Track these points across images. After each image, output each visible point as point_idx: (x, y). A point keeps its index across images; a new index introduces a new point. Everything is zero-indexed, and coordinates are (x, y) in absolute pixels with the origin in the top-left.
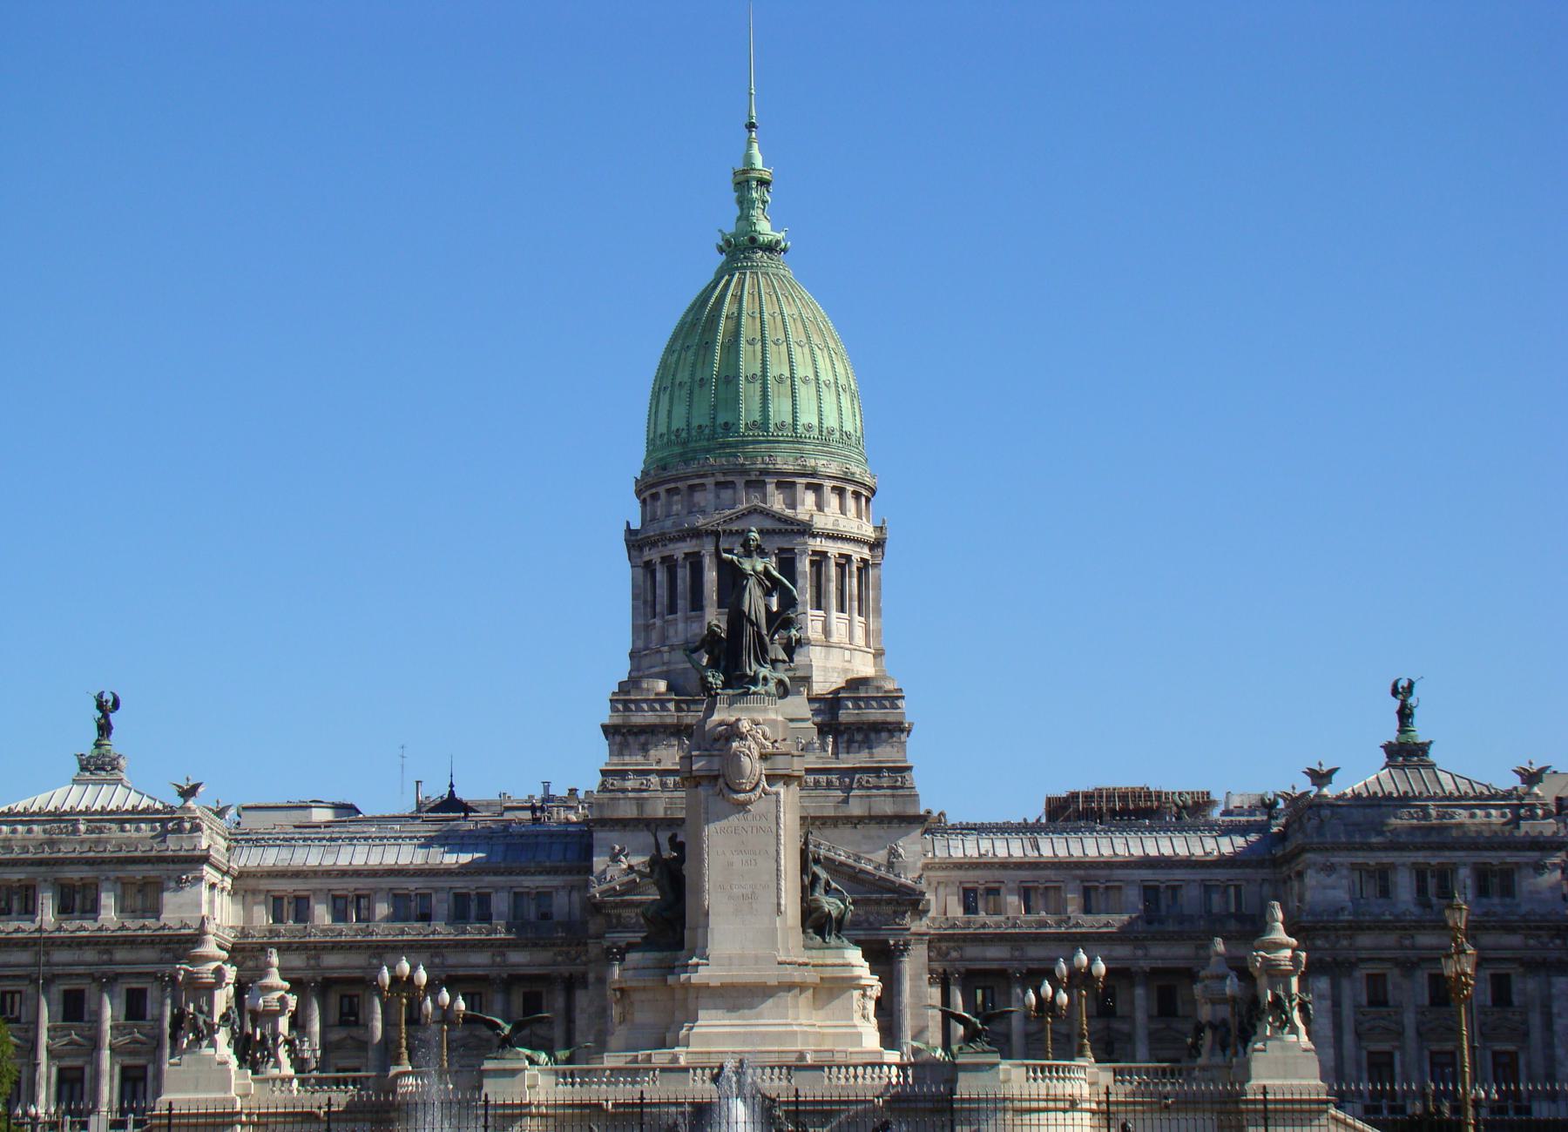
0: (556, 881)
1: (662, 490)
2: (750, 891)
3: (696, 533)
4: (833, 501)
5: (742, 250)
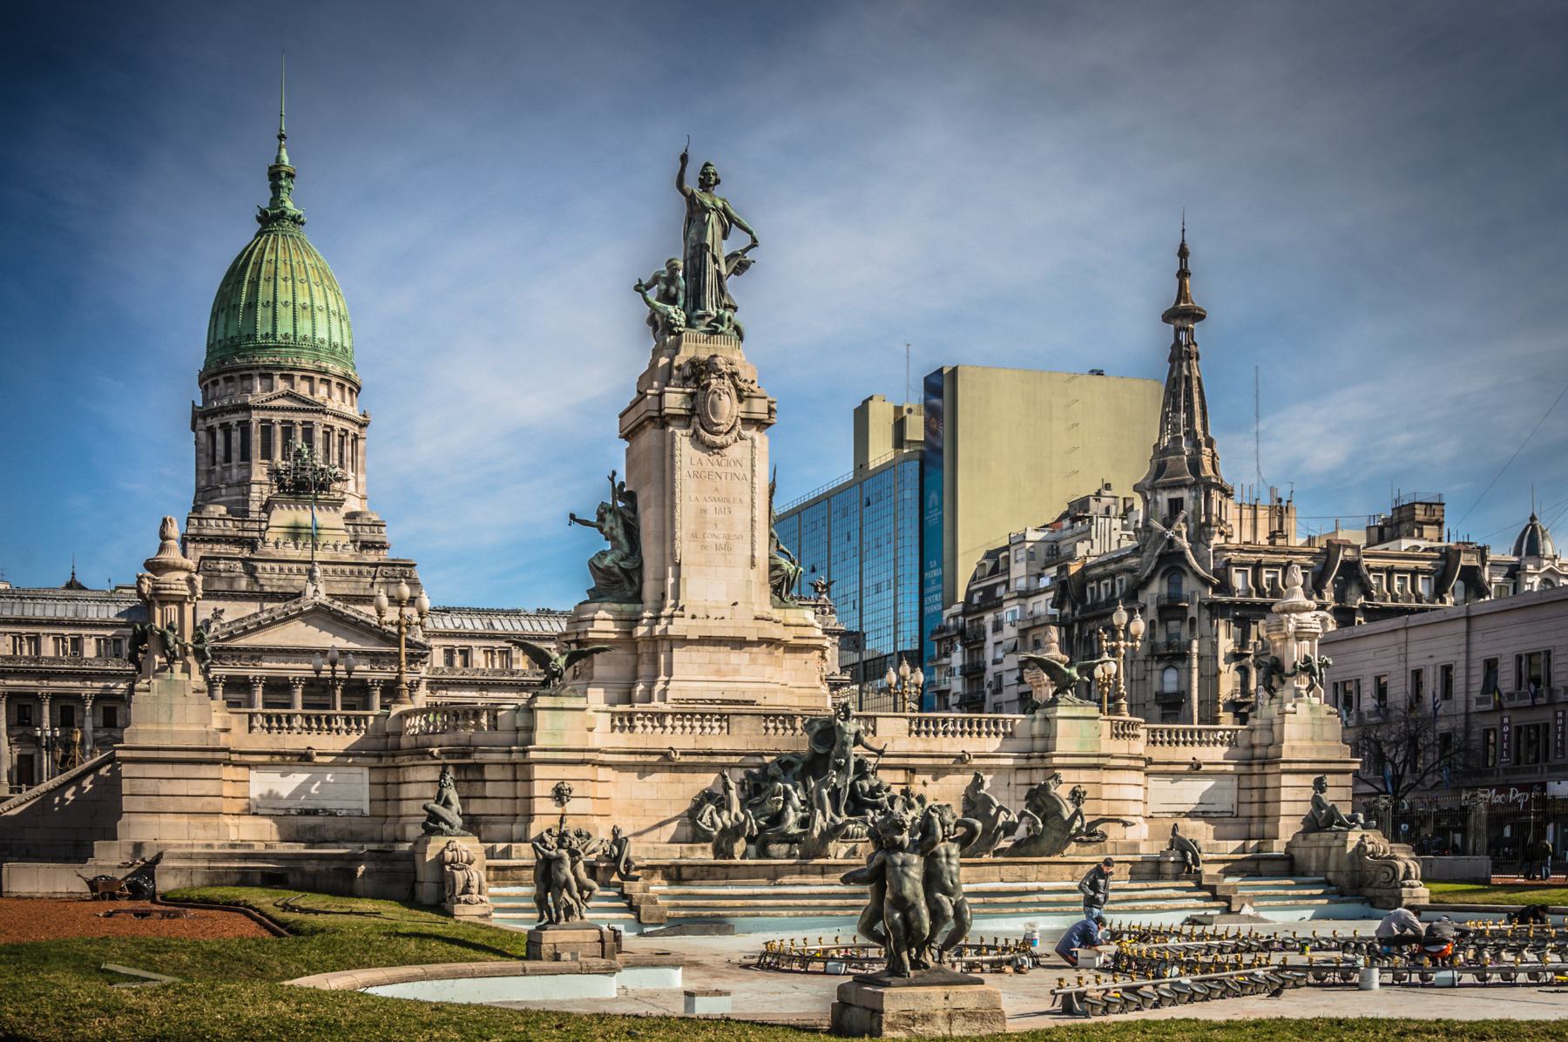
1: (220, 378)
2: (723, 541)
4: (337, 393)
5: (271, 220)
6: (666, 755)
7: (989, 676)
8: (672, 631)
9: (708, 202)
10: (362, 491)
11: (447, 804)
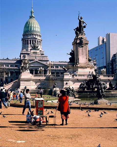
0: (19, 64)
3: (28, 38)
6: (78, 79)
7: (114, 69)
8: (78, 66)
9: (81, 20)
10: (41, 48)
11: (56, 85)
